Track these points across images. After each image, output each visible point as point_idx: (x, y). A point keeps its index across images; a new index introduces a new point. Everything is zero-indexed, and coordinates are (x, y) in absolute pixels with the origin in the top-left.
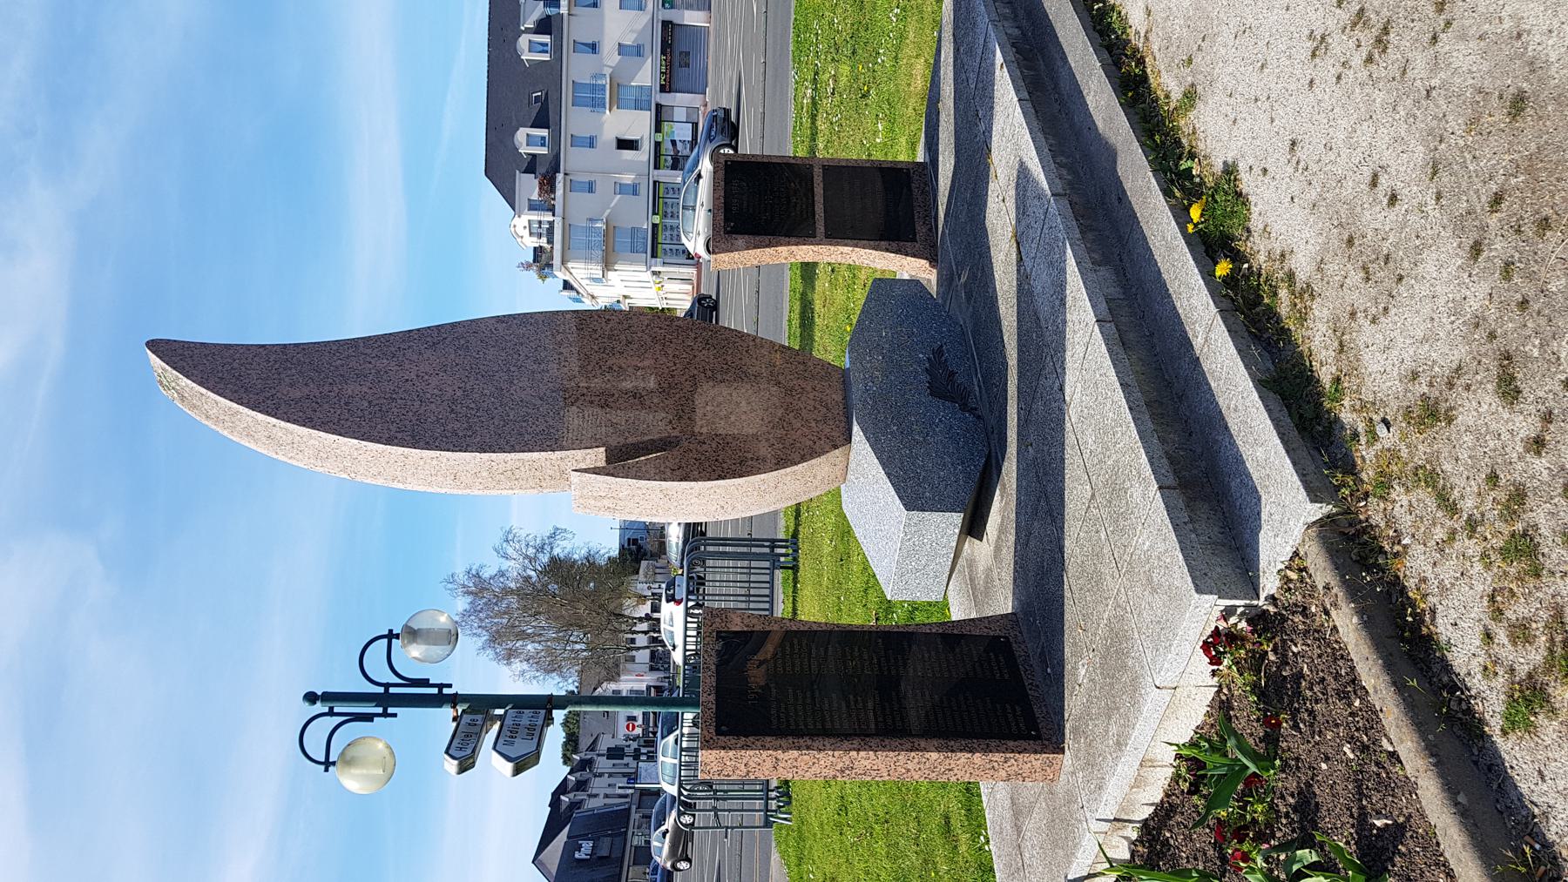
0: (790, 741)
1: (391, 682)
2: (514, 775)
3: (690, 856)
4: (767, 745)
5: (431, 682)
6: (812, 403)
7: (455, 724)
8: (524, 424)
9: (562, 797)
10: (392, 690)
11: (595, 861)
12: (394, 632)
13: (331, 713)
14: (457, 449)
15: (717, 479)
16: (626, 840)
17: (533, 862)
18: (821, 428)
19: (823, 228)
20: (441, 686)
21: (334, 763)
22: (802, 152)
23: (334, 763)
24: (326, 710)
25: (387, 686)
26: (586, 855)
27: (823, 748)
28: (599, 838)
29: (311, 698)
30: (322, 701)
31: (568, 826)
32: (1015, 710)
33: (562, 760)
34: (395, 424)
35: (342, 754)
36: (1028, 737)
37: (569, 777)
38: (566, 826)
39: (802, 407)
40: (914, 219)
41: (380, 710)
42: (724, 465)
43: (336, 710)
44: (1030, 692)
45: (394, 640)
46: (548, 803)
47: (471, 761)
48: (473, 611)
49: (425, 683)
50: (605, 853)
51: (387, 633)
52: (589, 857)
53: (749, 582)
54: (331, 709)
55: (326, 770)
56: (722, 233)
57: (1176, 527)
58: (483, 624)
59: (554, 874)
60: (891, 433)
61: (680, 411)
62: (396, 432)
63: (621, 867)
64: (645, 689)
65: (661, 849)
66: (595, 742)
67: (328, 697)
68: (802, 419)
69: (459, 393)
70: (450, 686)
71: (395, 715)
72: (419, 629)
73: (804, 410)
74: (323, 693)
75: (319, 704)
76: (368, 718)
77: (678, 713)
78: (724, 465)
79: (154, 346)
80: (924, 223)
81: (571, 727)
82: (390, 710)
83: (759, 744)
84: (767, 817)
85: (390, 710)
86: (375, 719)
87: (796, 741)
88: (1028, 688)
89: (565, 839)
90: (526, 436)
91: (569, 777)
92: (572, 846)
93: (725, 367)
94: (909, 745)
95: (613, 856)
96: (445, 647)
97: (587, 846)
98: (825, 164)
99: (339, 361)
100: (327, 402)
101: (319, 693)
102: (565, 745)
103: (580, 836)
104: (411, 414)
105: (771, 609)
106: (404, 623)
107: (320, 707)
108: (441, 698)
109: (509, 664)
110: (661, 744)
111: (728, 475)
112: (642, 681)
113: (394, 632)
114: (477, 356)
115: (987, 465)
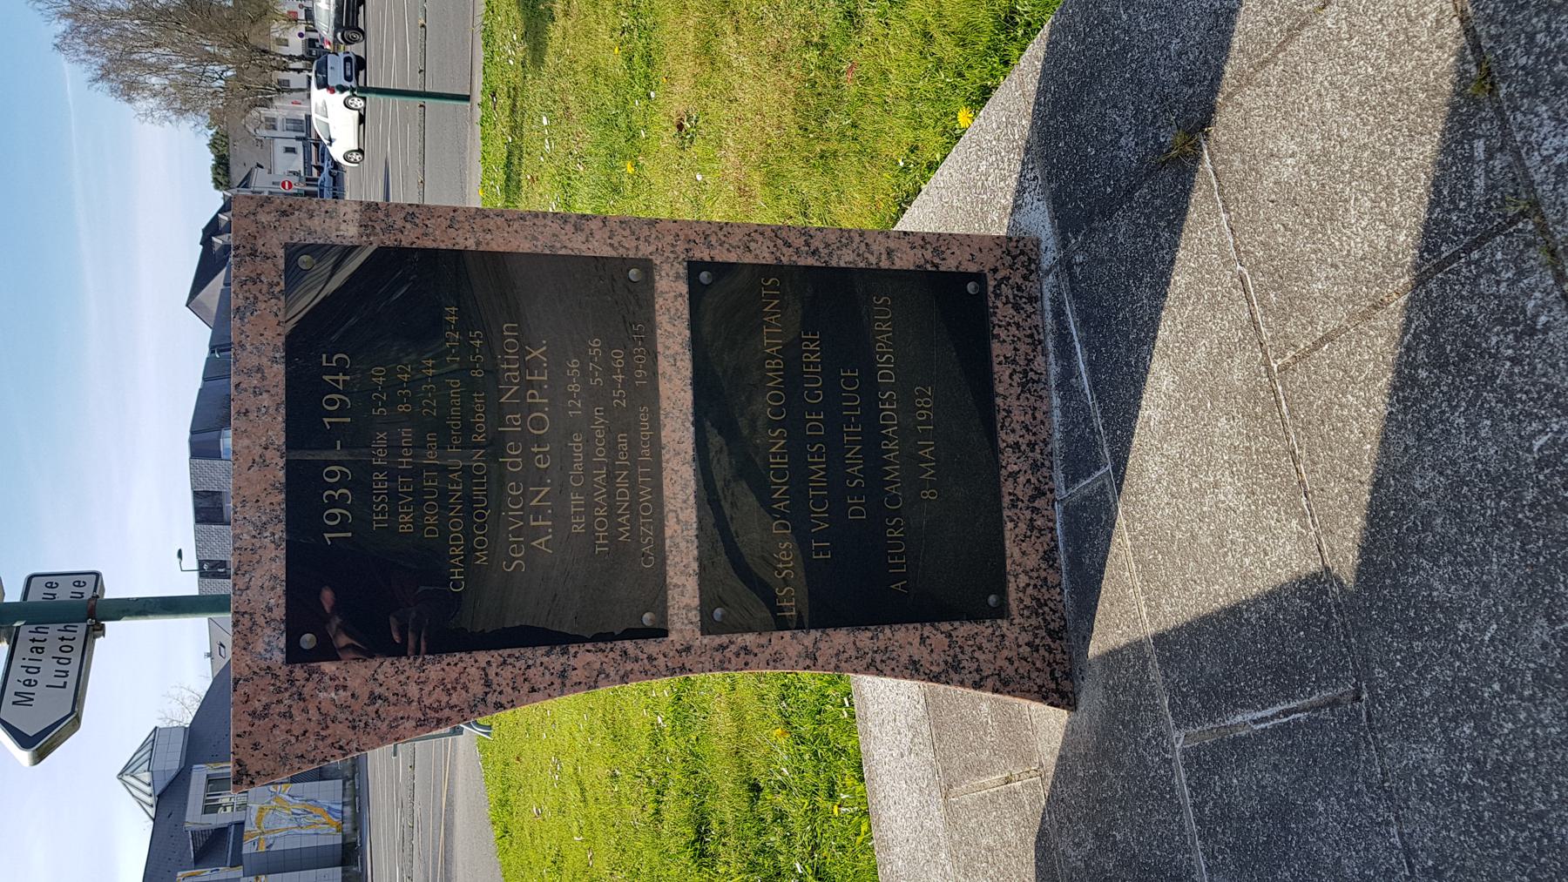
2: (36, 763)
3: (361, 26)
9: (214, 239)
33: (213, 184)
37: (220, 215)
38: (221, 269)
40: (1000, 510)
46: (199, 241)
48: (75, 30)
58: (92, 49)
59: (215, 310)
64: (304, 118)
66: (248, 177)
80: (1031, 527)
81: (220, 148)
91: (220, 215)
98: (701, 254)
102: (215, 168)
109: (130, 100)
112: (299, 109)
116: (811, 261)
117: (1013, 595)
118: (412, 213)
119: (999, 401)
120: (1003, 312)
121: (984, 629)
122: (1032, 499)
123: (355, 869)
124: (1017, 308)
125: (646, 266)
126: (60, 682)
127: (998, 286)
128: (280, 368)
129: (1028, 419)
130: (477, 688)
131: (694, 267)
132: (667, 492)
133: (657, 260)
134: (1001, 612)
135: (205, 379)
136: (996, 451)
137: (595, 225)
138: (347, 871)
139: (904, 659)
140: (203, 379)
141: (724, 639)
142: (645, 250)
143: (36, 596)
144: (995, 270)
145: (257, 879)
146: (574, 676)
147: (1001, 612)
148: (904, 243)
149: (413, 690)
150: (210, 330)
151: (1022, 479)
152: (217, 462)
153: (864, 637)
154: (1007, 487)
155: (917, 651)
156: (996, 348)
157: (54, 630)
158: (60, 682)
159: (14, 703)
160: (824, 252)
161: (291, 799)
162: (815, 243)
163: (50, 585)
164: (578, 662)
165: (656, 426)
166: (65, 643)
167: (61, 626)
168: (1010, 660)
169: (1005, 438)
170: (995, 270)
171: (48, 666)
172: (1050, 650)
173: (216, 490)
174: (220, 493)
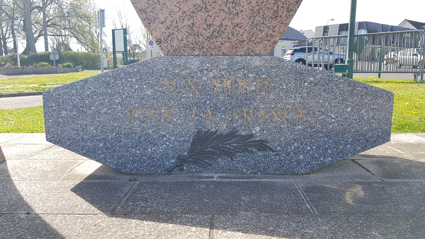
6: (217, 22)
18: (183, 30)
39: (210, 13)
60: (142, 89)
68: (193, 12)
73: (206, 14)
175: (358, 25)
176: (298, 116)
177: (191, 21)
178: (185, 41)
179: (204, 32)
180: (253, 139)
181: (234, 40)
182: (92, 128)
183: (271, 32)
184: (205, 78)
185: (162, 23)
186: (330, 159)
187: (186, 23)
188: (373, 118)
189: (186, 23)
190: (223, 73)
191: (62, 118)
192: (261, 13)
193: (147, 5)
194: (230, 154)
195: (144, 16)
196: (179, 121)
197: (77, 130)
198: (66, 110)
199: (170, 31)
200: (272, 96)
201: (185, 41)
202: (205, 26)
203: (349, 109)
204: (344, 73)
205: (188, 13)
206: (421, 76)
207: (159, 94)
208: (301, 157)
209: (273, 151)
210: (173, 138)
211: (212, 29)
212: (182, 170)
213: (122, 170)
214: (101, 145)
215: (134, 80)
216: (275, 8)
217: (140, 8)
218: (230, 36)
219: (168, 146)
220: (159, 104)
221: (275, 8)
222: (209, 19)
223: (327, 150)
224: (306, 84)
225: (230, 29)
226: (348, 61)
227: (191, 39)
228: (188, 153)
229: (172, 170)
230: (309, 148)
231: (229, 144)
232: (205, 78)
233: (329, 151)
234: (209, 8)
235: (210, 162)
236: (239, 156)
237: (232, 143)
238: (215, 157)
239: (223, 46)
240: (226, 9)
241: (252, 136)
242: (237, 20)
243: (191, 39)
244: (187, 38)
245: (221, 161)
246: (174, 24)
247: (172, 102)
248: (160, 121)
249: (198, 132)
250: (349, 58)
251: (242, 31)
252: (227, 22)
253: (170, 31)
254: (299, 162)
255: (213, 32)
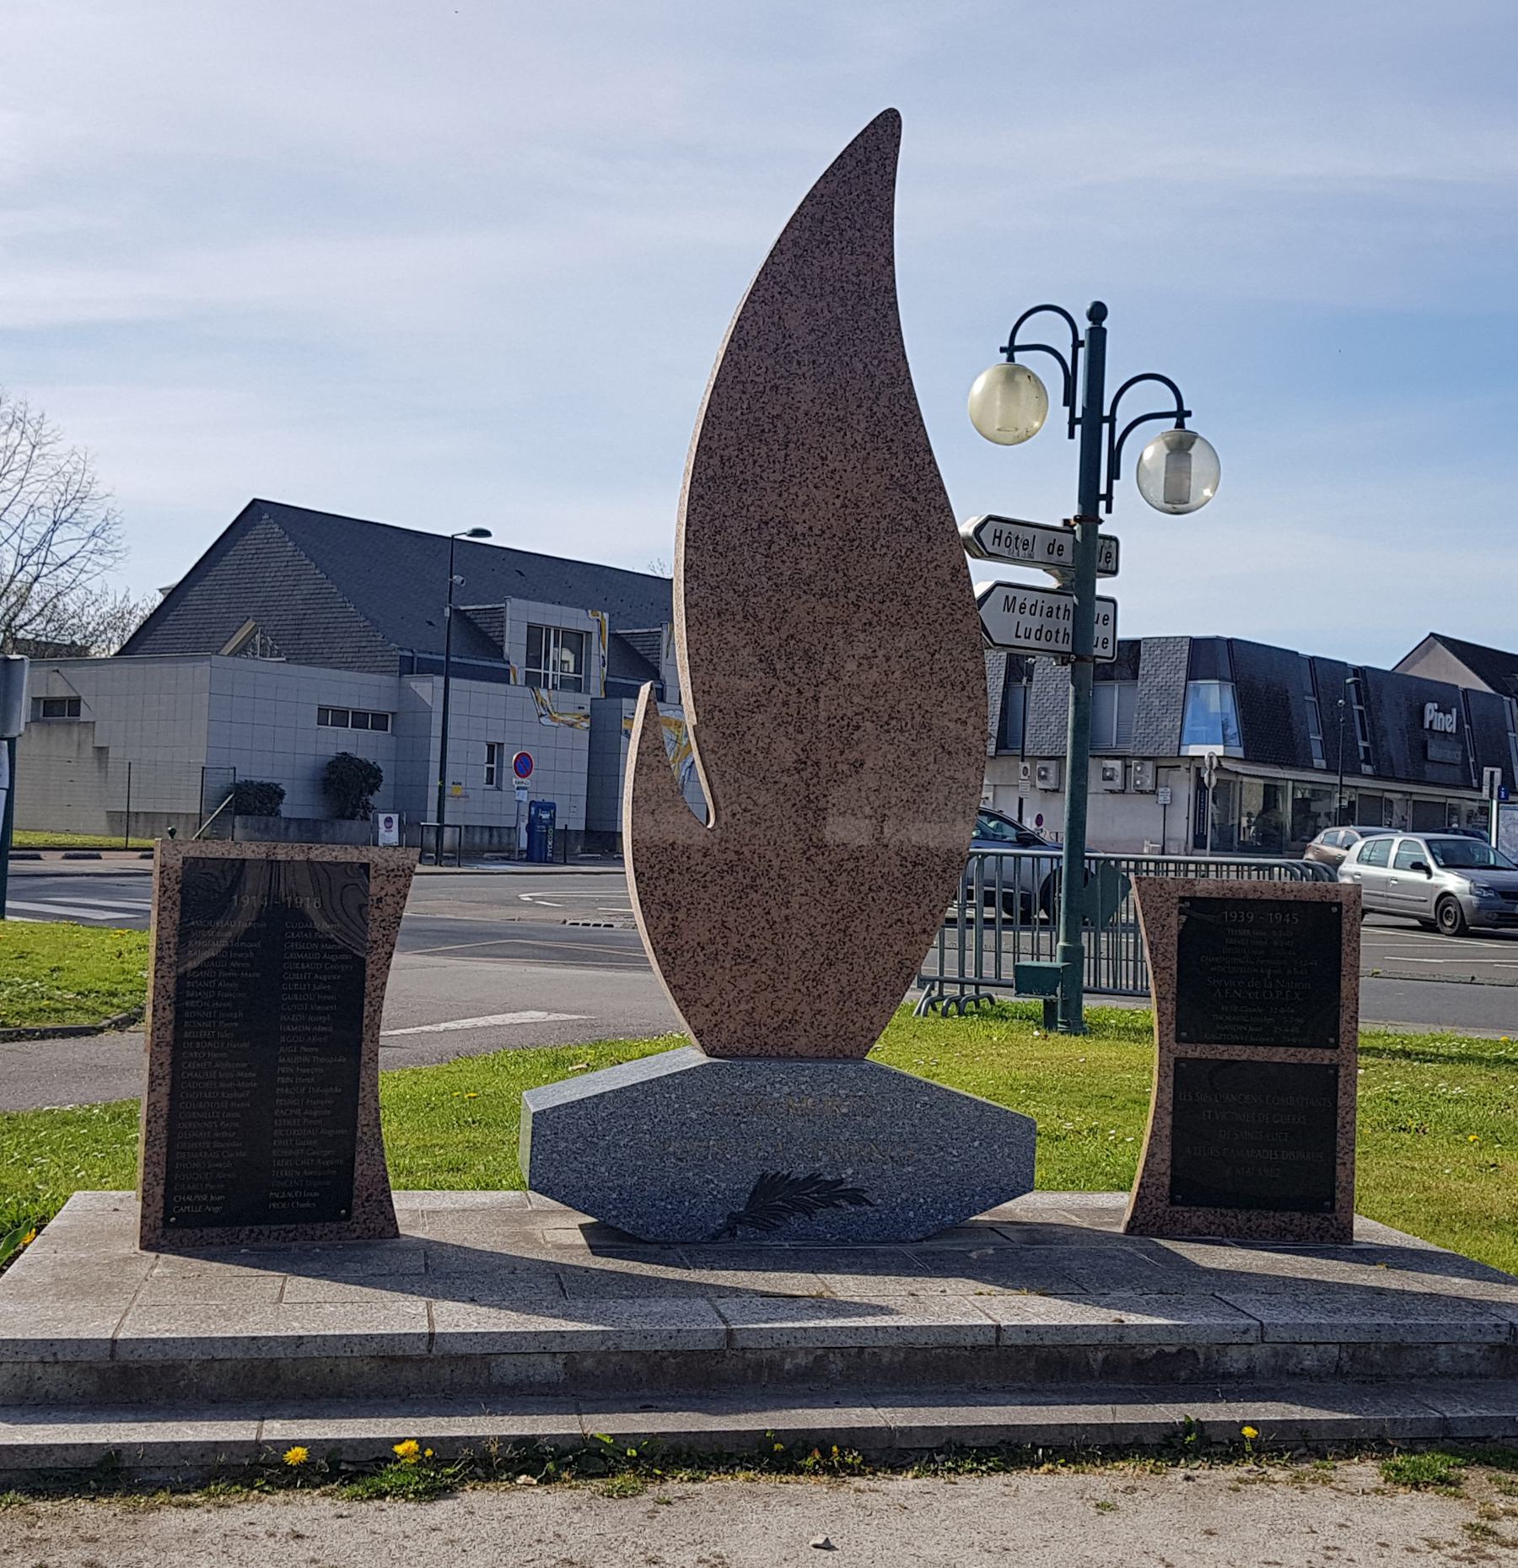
0: (171, 939)
1: (1117, 424)
4: (165, 914)
5: (1115, 482)
6: (789, 1007)
7: (1059, 524)
8: (739, 618)
10: (1106, 427)
11: (1419, 738)
12: (1186, 420)
13: (1077, 344)
14: (691, 536)
15: (636, 871)
16: (1457, 787)
17: (1432, 635)
18: (738, 1018)
19: (1196, 1055)
20: (1108, 497)
21: (1011, 359)
22: (1368, 1029)
23: (1011, 359)
24: (1082, 336)
25: (1112, 420)
26: (1431, 722)
27: (159, 975)
28: (1461, 742)
29: (1098, 312)
30: (1091, 329)
31: (1484, 687)
32: (215, 1204)
34: (736, 453)
35: (1023, 369)
36: (167, 1210)
39: (780, 994)
41: (1079, 414)
42: (662, 881)
43: (1082, 351)
44: (247, 1228)
45: (1173, 421)
47: (978, 553)
49: (1114, 474)
50: (1433, 752)
51: (1186, 408)
52: (1427, 726)
53: (1127, 960)
54: (1082, 344)
55: (1002, 350)
56: (1182, 894)
57: (51, 1343)
59: (1410, 673)
60: (683, 1110)
61: (768, 823)
62: (722, 457)
63: (1408, 781)
65: (1334, 844)
67: (1098, 337)
68: (755, 992)
69: (799, 529)
70: (1109, 510)
71: (1071, 435)
72: (1190, 456)
73: (773, 995)
74: (1104, 331)
75: (1089, 324)
76: (1069, 400)
77: (1061, 849)
78: (662, 881)
79: (886, 128)
82: (1078, 428)
83: (169, 904)
84: (933, 980)
85: (1078, 428)
86: (1067, 409)
87: (171, 946)
88: (256, 1229)
89: (1462, 685)
90: (717, 621)
92: (1447, 696)
93: (865, 889)
94: (158, 1072)
95: (1427, 767)
96: (1162, 496)
97: (1447, 723)
98: (1342, 1072)
99: (861, 366)
100: (777, 363)
101: (1105, 324)
103: (1468, 710)
104: (758, 470)
105: (1097, 991)
106: (1200, 434)
107: (1084, 325)
108: (1092, 497)
110: (1419, 839)
111: (643, 885)
113: (1186, 420)
114: (878, 546)
115: (633, 1239)
116: (1339, 1124)
117: (1180, 1208)
118: (1357, 950)
119: (1272, 1213)
120: (1315, 1222)
121: (1165, 1192)
122: (1224, 1225)
123: (579, 848)
124: (1318, 1229)
125: (1336, 1046)
126: (1021, 633)
127: (1329, 1220)
128: (1292, 898)
129: (1262, 1228)
130: (1162, 965)
131: (1336, 1068)
132: (1236, 1047)
133: (1338, 1051)
134: (1173, 1203)
135: (1313, 660)
136: (1248, 1208)
137: (1354, 1025)
138: (576, 838)
139: (1156, 1150)
140: (1313, 658)
141: (1172, 1067)
142: (1343, 1046)
143: (1100, 609)
144: (1336, 1219)
145: (586, 717)
146: (1163, 1003)
147: (1173, 1203)
148: (1348, 1172)
149: (1165, 940)
150: (1389, 668)
151: (1234, 1221)
152: (1183, 674)
153: (1167, 1131)
154: (1231, 1213)
155: (1159, 1157)
156: (1298, 1215)
157: (1068, 625)
158: (1021, 633)
159: (1007, 597)
160: (1344, 1131)
161: (687, 764)
162: (1348, 1126)
163: (1106, 618)
164: (1169, 1005)
165: (1264, 1044)
166: (1054, 635)
167: (1070, 631)
168: (1151, 1203)
169: (1254, 1213)
170: (1336, 1219)
171: (1034, 622)
172: (1154, 1224)
173: (1141, 672)
174: (1135, 676)
175: (1185, 655)
176: (908, 1153)
177: (751, 1005)
178: (739, 1034)
179: (769, 1020)
180: (842, 1187)
181: (814, 1033)
182: (603, 1169)
183: (867, 1024)
184: (776, 1095)
185: (707, 1006)
186: (951, 1217)
187: (743, 1006)
188: (1009, 1156)
189: (743, 1006)
190: (803, 1087)
191: (559, 1153)
192: (854, 997)
193: (686, 979)
194: (808, 1211)
195: (680, 995)
196: (735, 1159)
197: (579, 1172)
198: (567, 1141)
199: (718, 1018)
200: (871, 1122)
201: (739, 1034)
202: (771, 1013)
203: (976, 1144)
204: (1048, 998)
205: (747, 993)
206: (589, 1261)
207: (708, 1117)
208: (911, 1214)
209: (871, 1205)
210: (724, 1185)
211: (781, 1017)
212: (735, 1235)
213: (642, 1237)
214: (614, 1196)
215: (673, 1096)
216: (874, 990)
217: (674, 983)
218: (808, 1028)
219: (715, 1196)
220: (707, 1133)
221: (874, 990)
222: (778, 1002)
223: (946, 1203)
224: (918, 1106)
225: (807, 1018)
226: (1064, 949)
227: (748, 1031)
228: (746, 1208)
229: (720, 1236)
230: (922, 1200)
231: (807, 1195)
232: (776, 1095)
233: (950, 1206)
234: (779, 986)
235: (777, 1223)
236: (823, 1213)
237: (813, 1192)
238: (785, 1215)
239: (797, 1043)
240: (804, 989)
241: (842, 1181)
242: (818, 1005)
243: (748, 1031)
244: (743, 1030)
245: (796, 1222)
246: (725, 1008)
247: (727, 1130)
248: (706, 1158)
249: (762, 1176)
250: (1066, 940)
251: (825, 1020)
252: (804, 1007)
253: (718, 1018)
254: (908, 1222)
255: (784, 1021)
